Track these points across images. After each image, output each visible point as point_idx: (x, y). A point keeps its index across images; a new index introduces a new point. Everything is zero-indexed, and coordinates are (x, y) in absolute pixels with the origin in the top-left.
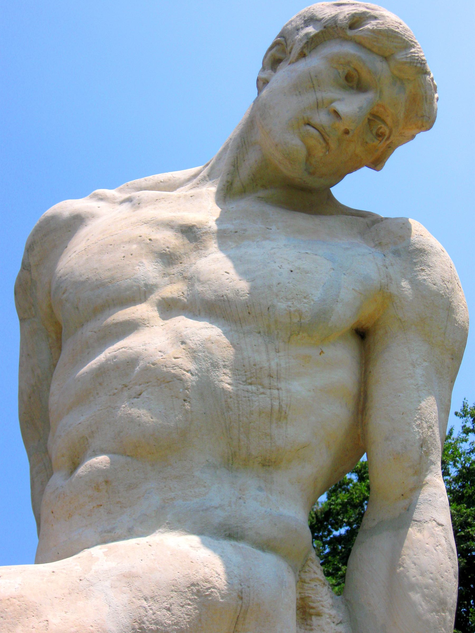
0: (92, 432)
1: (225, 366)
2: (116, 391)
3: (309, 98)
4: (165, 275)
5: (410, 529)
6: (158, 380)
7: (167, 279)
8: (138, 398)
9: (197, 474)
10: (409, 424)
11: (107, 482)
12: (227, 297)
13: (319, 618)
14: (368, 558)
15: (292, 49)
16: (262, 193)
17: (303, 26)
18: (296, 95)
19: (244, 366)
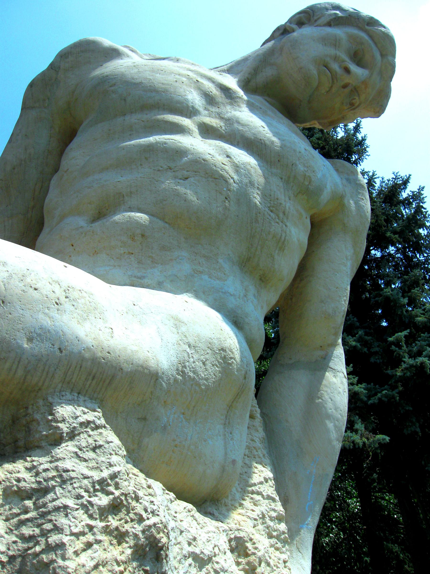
0: (131, 192)
2: (161, 169)
3: (332, 51)
4: (206, 109)
5: (327, 373)
6: (207, 173)
8: (184, 180)
9: (220, 261)
11: (143, 236)
12: (264, 141)
13: (253, 420)
14: (290, 387)
15: (319, 19)
17: (331, 8)
18: (322, 45)
19: (270, 195)
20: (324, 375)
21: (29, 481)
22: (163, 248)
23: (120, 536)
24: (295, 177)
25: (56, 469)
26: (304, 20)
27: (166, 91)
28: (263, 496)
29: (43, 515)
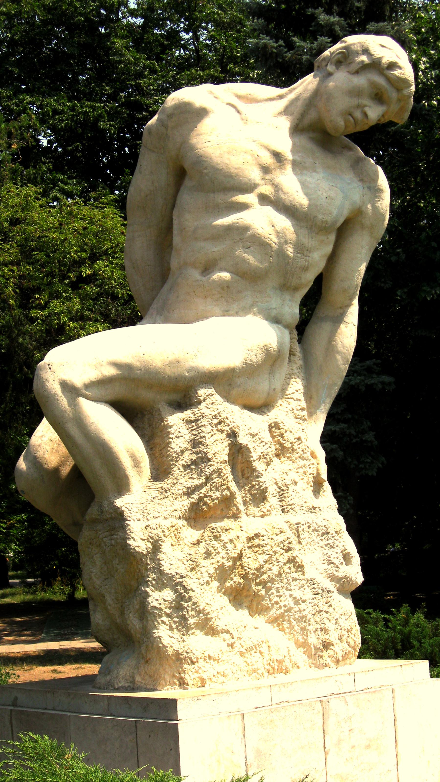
1: (290, 243)
3: (355, 101)
7: (263, 181)
10: (354, 277)
11: (228, 287)
14: (318, 332)
16: (311, 135)
20: (339, 326)
21: (193, 418)
22: (239, 292)
23: (222, 431)
24: (316, 224)
25: (200, 413)
26: (342, 60)
27: (237, 175)
28: (294, 399)
29: (198, 428)
